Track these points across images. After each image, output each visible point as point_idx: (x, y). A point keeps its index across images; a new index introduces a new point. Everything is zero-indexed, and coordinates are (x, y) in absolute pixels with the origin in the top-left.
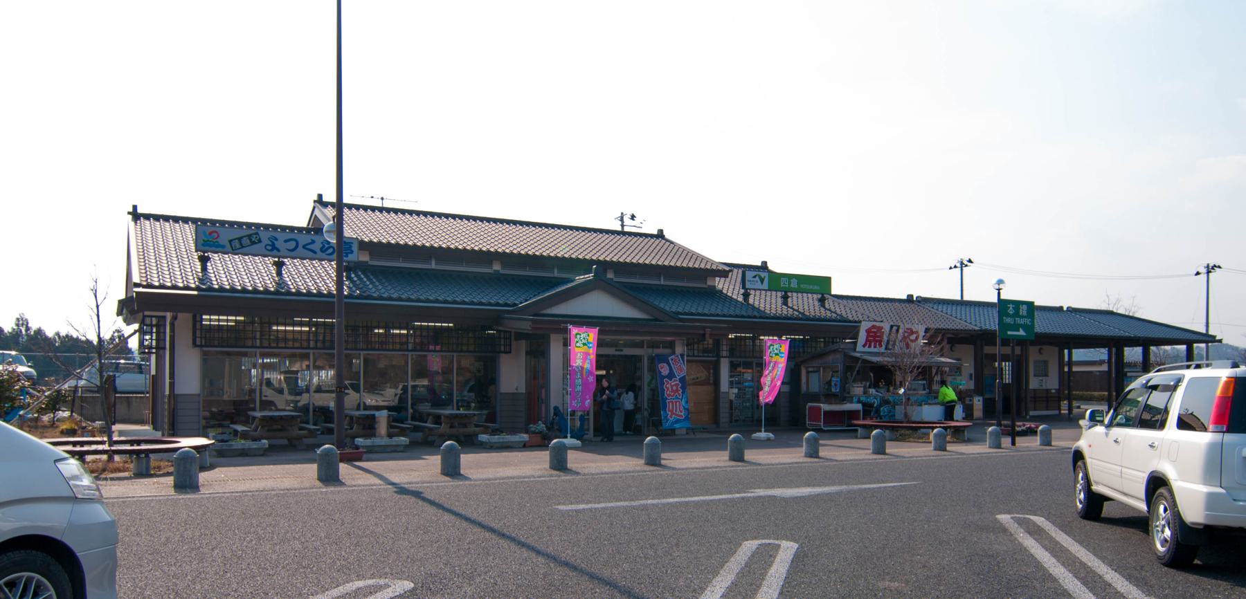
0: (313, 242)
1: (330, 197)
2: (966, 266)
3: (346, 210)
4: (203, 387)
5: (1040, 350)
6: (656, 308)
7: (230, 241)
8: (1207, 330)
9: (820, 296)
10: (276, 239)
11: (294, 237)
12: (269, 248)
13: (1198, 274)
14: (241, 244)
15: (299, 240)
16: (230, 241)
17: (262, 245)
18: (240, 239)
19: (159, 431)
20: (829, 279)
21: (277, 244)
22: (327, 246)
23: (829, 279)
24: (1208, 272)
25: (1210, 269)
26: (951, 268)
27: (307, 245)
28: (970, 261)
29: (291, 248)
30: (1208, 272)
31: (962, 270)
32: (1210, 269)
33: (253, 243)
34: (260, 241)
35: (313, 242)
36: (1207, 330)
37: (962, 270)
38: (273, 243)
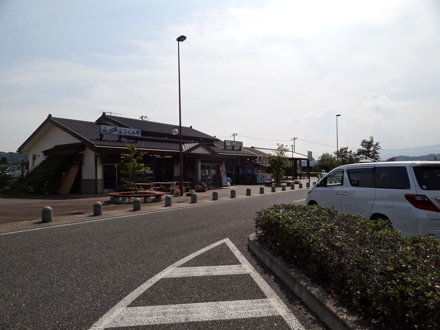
0: (130, 131)
1: (288, 150)
2: (236, 136)
3: (292, 151)
4: (110, 200)
5: (241, 255)
6: (213, 151)
7: (110, 130)
8: (234, 140)
9: (232, 147)
10: (121, 130)
11: (126, 129)
12: (119, 132)
13: (292, 140)
14: (112, 131)
15: (127, 130)
16: (110, 130)
17: (118, 131)
18: (112, 129)
19: (290, 186)
20: (242, 142)
21: (121, 131)
22: (133, 132)
23: (242, 142)
24: (294, 140)
25: (295, 139)
26: (231, 136)
27: (129, 131)
28: (237, 134)
29: (125, 133)
30: (294, 140)
31: (234, 137)
32: (295, 139)
33: (115, 131)
34: (117, 130)
35: (130, 131)
36: (234, 140)
37: (234, 137)
38: (120, 131)
